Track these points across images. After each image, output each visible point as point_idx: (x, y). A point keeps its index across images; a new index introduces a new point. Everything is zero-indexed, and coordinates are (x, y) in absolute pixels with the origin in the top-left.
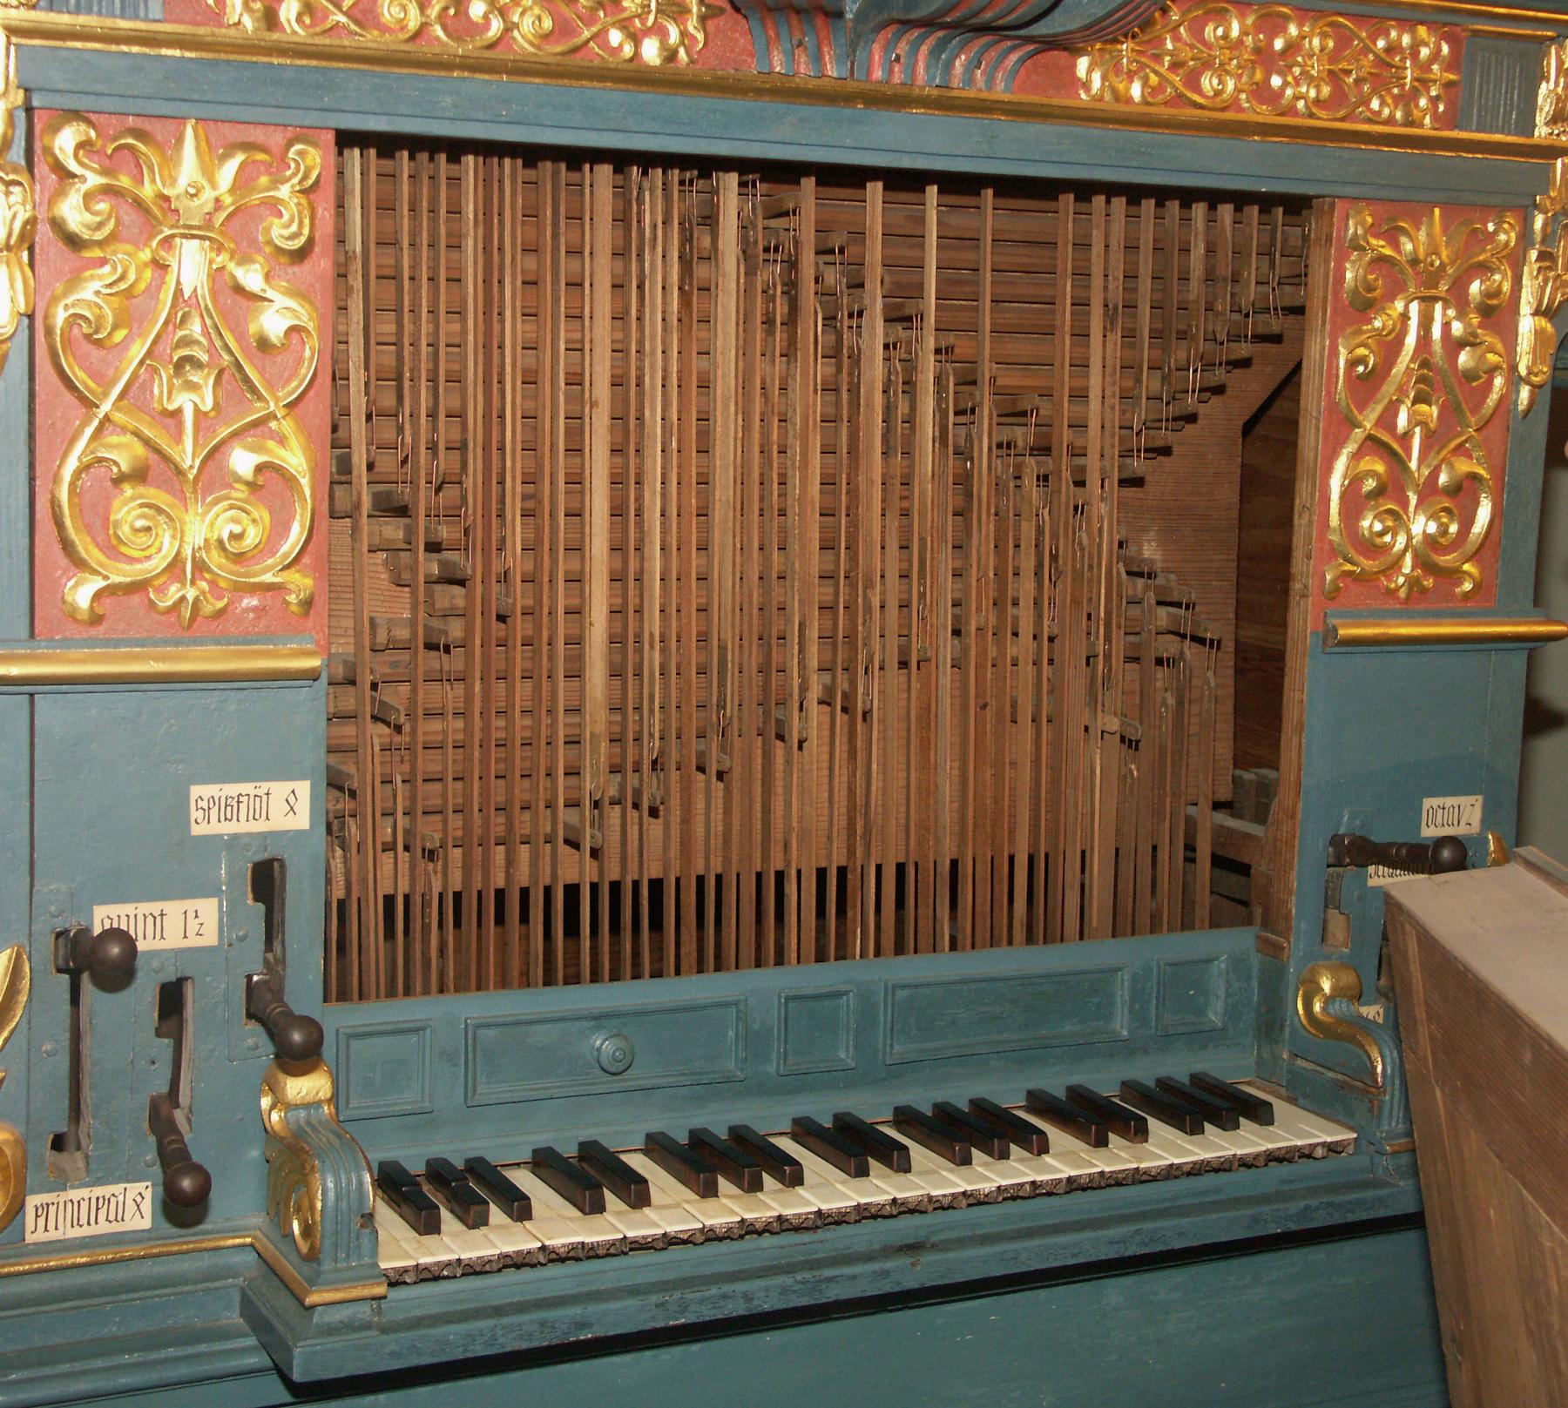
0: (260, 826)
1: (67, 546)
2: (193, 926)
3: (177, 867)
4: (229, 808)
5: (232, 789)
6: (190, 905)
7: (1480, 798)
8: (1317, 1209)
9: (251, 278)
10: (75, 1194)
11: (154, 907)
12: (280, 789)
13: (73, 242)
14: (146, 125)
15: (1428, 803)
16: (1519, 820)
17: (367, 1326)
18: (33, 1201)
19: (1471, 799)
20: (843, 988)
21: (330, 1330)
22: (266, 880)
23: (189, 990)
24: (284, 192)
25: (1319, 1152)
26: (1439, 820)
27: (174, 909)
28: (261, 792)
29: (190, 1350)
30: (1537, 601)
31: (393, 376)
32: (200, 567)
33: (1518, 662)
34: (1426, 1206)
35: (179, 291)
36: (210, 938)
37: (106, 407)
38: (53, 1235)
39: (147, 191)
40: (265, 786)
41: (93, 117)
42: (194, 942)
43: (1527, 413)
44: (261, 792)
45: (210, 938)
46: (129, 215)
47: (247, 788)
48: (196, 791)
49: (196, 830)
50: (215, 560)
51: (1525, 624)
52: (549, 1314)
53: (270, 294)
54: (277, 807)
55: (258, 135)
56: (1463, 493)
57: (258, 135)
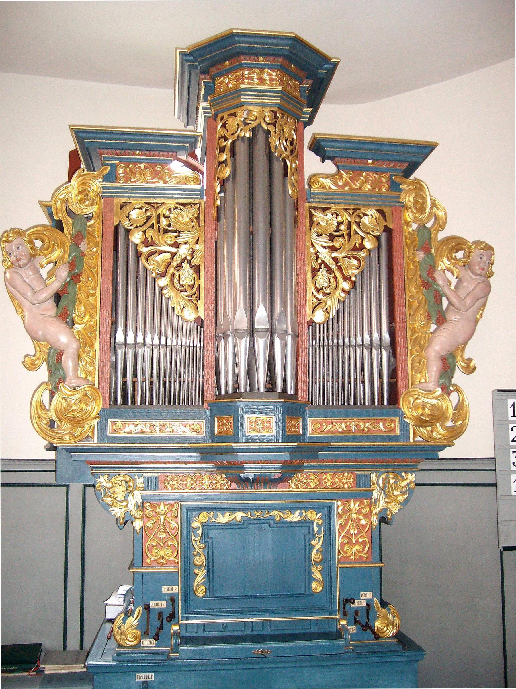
0: (171, 592)
1: (147, 555)
3: (160, 597)
4: (167, 589)
9: (361, 517)
10: (148, 640)
12: (174, 587)
13: (148, 517)
15: (361, 593)
16: (270, 193)
20: (314, 314)
22: (173, 600)
24: (174, 510)
27: (160, 602)
31: (391, 208)
32: (163, 557)
34: (281, 180)
36: (165, 607)
37: (151, 537)
39: (157, 511)
45: (165, 607)
46: (154, 513)
49: (163, 592)
50: (165, 556)
53: (172, 522)
56: (364, 543)
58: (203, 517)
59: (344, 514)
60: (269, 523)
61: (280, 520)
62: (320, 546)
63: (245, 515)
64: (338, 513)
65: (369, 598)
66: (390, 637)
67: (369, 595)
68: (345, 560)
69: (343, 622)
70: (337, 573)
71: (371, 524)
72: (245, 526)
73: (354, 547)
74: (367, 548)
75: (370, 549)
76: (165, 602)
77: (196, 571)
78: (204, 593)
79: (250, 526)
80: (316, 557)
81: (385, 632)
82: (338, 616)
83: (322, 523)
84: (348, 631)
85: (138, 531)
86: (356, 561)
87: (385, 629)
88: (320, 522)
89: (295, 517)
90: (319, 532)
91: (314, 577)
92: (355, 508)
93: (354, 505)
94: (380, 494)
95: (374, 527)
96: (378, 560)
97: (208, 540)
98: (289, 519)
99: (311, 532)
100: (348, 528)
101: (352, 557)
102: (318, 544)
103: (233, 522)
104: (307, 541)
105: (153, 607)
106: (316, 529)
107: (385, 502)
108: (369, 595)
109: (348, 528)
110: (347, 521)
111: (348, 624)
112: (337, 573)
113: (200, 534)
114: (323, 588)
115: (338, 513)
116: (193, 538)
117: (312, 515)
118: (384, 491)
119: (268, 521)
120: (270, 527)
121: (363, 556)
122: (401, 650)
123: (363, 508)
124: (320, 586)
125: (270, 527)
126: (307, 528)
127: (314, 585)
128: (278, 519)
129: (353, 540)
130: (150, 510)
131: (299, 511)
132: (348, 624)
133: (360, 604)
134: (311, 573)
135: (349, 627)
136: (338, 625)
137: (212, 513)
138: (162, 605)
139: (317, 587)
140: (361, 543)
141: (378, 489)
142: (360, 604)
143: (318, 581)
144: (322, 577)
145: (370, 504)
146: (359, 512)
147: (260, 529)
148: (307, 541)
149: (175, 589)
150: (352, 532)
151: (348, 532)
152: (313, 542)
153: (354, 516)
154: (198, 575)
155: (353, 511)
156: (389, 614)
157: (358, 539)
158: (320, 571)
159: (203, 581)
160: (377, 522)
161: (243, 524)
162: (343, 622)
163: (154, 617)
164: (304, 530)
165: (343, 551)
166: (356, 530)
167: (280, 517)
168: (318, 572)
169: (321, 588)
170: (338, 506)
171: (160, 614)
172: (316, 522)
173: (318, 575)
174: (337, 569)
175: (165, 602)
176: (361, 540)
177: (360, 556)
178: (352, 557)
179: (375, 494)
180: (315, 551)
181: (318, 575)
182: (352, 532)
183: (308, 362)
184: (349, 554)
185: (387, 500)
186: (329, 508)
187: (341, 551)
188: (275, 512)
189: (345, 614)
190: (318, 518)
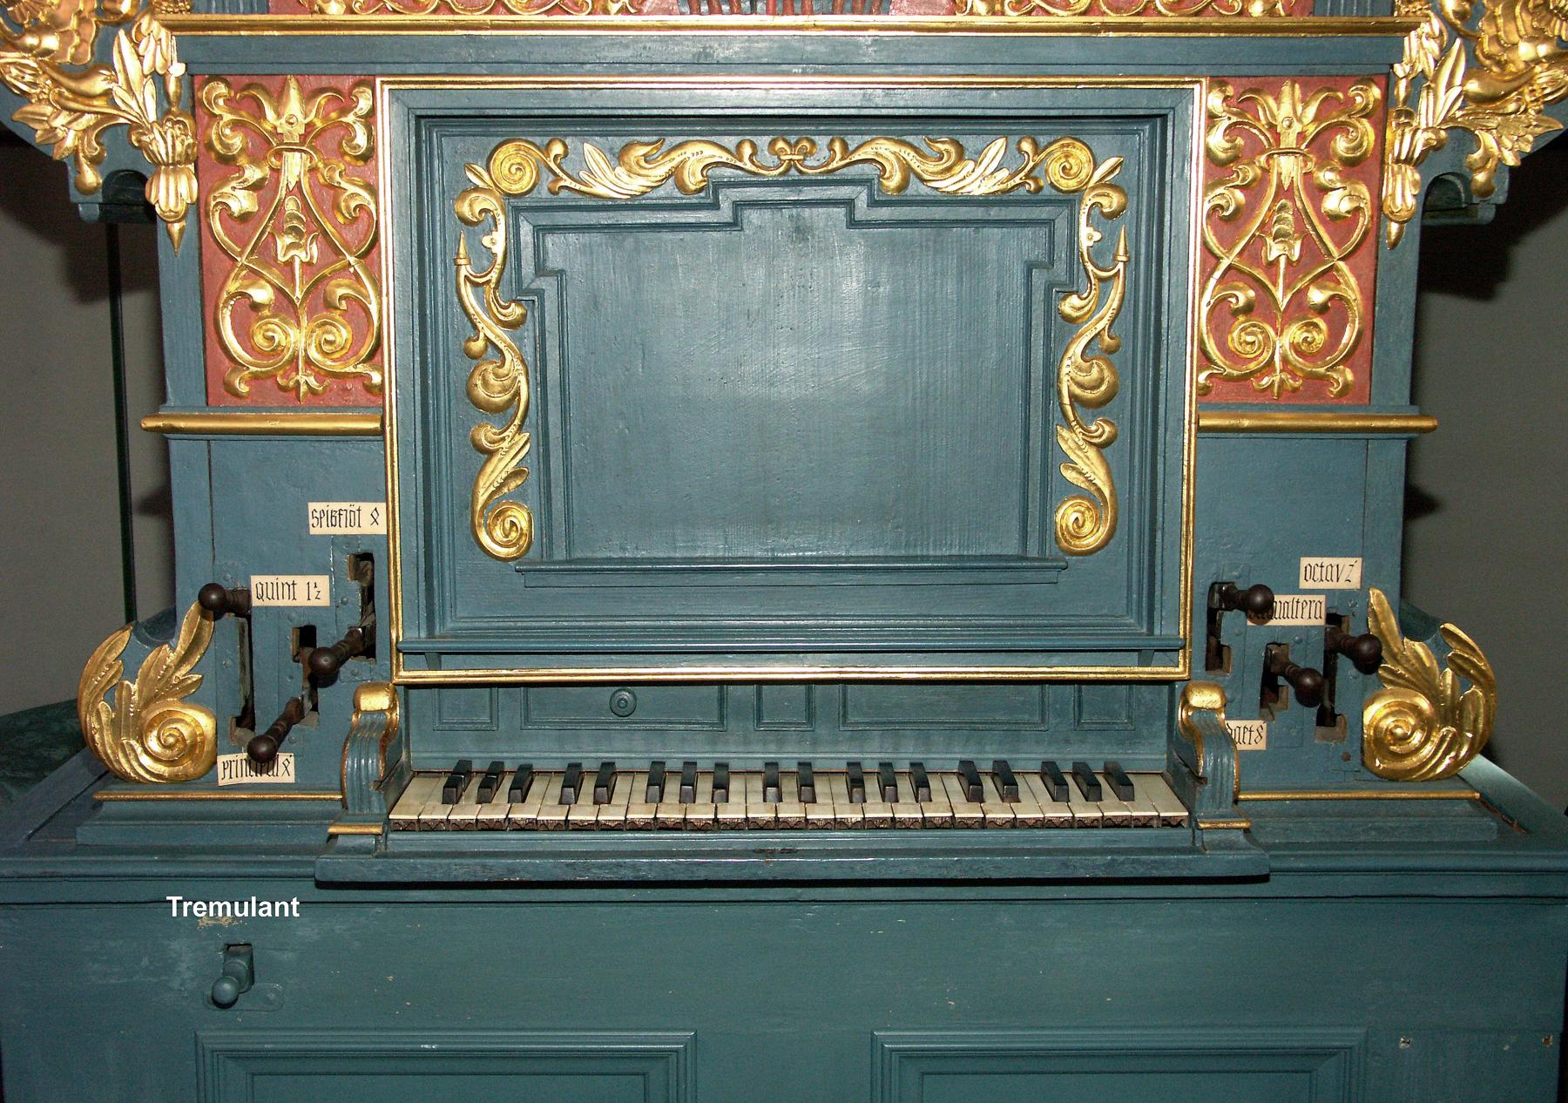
2: (313, 592)
3: (301, 555)
5: (335, 506)
6: (312, 579)
7: (1360, 560)
8: (1123, 863)
9: (1326, 177)
11: (289, 579)
12: (367, 508)
14: (256, 80)
15: (1305, 561)
17: (368, 851)
18: (221, 759)
19: (1352, 560)
21: (345, 851)
23: (123, 620)
24: (350, 118)
25: (1155, 822)
26: (1317, 576)
27: (301, 581)
28: (355, 508)
29: (273, 858)
30: (1413, 399)
33: (1398, 450)
35: (1280, 185)
36: (325, 600)
38: (235, 781)
40: (357, 505)
41: (229, 79)
42: (314, 603)
43: (1394, 245)
44: (355, 508)
45: (325, 600)
47: (345, 505)
48: (312, 506)
49: (313, 531)
51: (1231, 417)
52: (490, 861)
54: (366, 519)
55: (333, 82)
56: (1334, 311)
57: (333, 82)
58: (514, 166)
59: (1235, 159)
60: (849, 203)
61: (903, 186)
62: (1105, 323)
63: (725, 157)
64: (1208, 151)
65: (1342, 585)
66: (1439, 778)
67: (1348, 572)
68: (1234, 387)
69: (1206, 698)
70: (1189, 456)
71: (1380, 211)
72: (725, 214)
73: (1279, 333)
74: (1349, 336)
75: (1366, 344)
76: (323, 582)
77: (486, 434)
78: (524, 542)
79: (753, 217)
80: (1081, 377)
81: (1418, 750)
82: (1179, 671)
83: (1122, 208)
84: (1227, 740)
85: (176, 228)
86: (1286, 398)
87: (1417, 737)
88: (1112, 201)
89: (983, 173)
90: (1100, 253)
91: (1070, 475)
92: (1297, 127)
93: (1290, 111)
94: (1445, 51)
95: (1394, 228)
96: (1406, 400)
97: (542, 283)
98: (948, 185)
99: (1061, 253)
100: (1253, 228)
101: (1266, 381)
102: (1095, 312)
103: (661, 192)
104: (1038, 296)
105: (267, 603)
106: (1087, 236)
107: (1467, 97)
108: (1348, 572)
109: (1253, 228)
110: (1253, 189)
111: (1231, 707)
112: (1189, 456)
113: (499, 249)
114: (1106, 543)
115: (1208, 151)
116: (463, 272)
117: (1070, 163)
118: (1465, 37)
119: (844, 192)
120: (853, 223)
121: (1322, 377)
122: (1485, 845)
123: (1341, 127)
124: (1098, 520)
125: (853, 223)
126: (1043, 232)
127: (1067, 514)
128: (894, 182)
129: (1279, 294)
130: (228, 117)
131: (1001, 142)
132: (1231, 707)
133: (1298, 613)
134: (1052, 457)
135: (1233, 724)
136: (1181, 714)
137: (557, 149)
138: (309, 592)
139: (1079, 524)
140: (1322, 310)
141: (1436, 24)
142: (1298, 613)
143: (1091, 496)
144: (1109, 473)
145: (1380, 116)
146: (1318, 146)
147: (801, 232)
148: (1038, 296)
149: (369, 520)
150: (1275, 250)
151: (1253, 251)
152: (1070, 305)
153: (1288, 168)
154: (490, 454)
155: (1289, 140)
156: (1442, 665)
157: (1303, 292)
158: (1100, 447)
159: (513, 485)
160: (1411, 202)
161: (715, 206)
162: (1206, 698)
163: (275, 649)
164: (1029, 243)
165: (1222, 346)
166: (1298, 245)
167: (907, 170)
168: (1092, 453)
169: (1103, 531)
170: (1212, 118)
171: (307, 635)
172: (1089, 200)
173: (1085, 465)
174: (1189, 438)
175: (323, 582)
176: (1317, 296)
177: (1311, 377)
178: (1266, 381)
179: (1420, 49)
180: (1077, 348)
181: (1085, 465)
182: (1275, 250)
183: (1127, 414)
184: (1253, 366)
185: (1473, 86)
186: (1157, 122)
187: (1211, 347)
188: (884, 148)
189: (1216, 658)
190: (1101, 184)
